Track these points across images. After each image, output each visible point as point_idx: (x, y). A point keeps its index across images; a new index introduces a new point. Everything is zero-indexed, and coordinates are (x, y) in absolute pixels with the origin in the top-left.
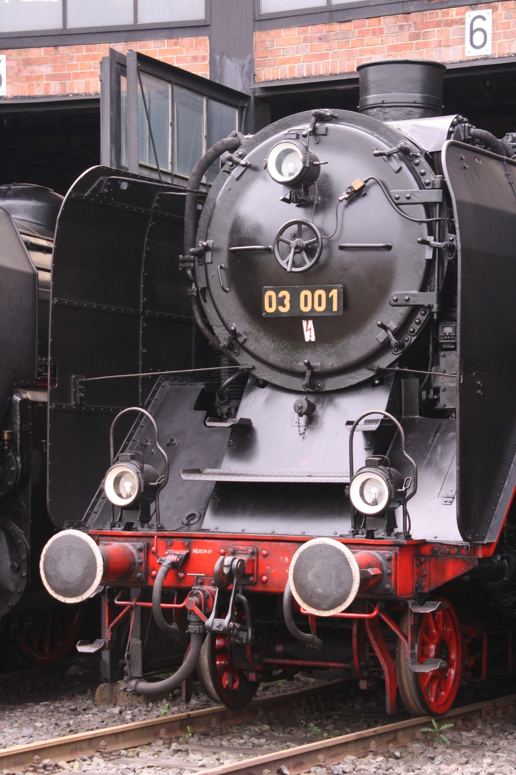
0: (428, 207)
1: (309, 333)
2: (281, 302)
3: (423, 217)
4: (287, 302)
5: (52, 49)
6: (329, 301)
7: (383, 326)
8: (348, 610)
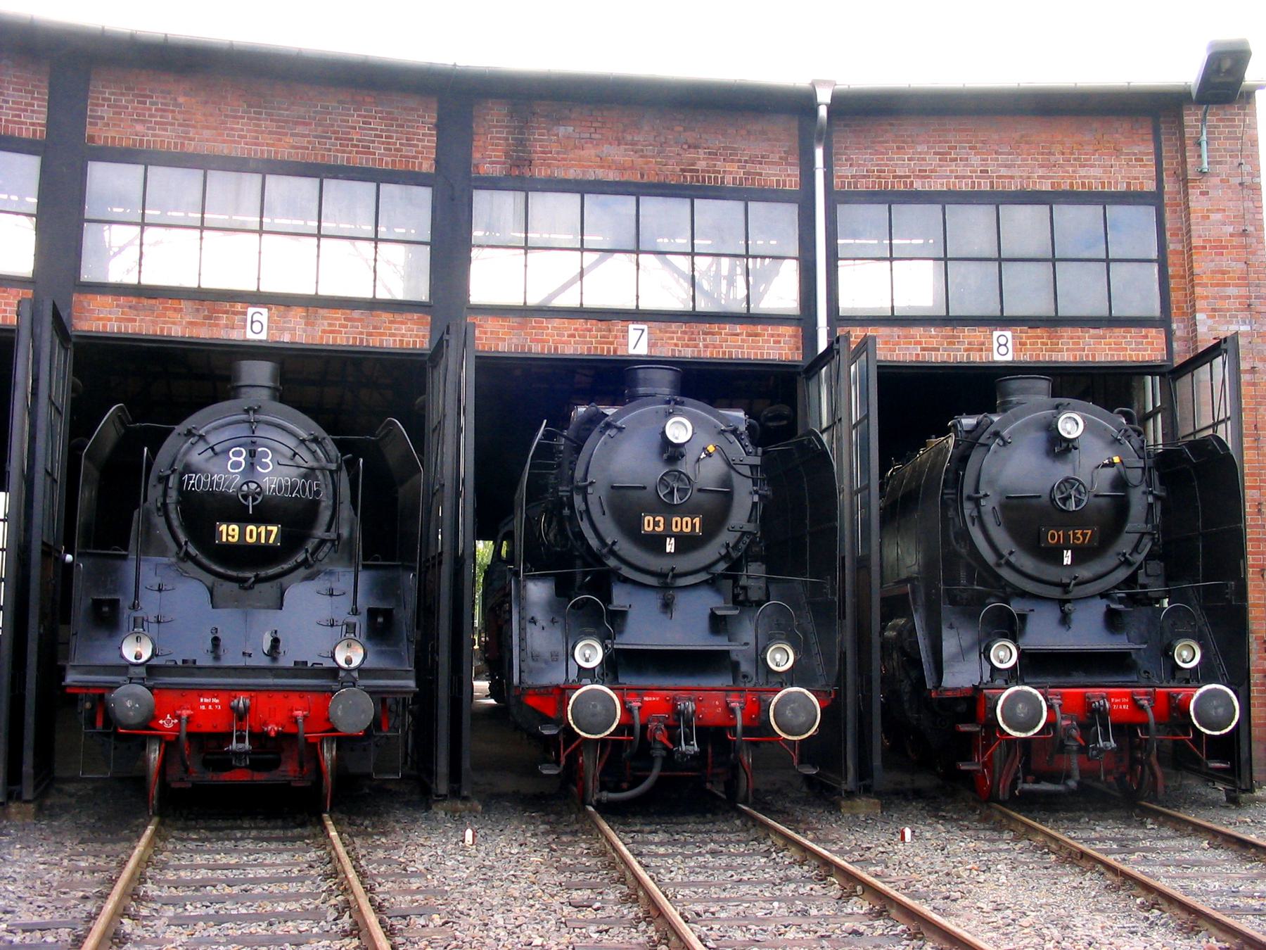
0: (752, 467)
1: (670, 546)
2: (656, 524)
3: (749, 474)
4: (661, 524)
5: (282, 308)
6: (693, 526)
7: (1011, 553)
8: (611, 734)
